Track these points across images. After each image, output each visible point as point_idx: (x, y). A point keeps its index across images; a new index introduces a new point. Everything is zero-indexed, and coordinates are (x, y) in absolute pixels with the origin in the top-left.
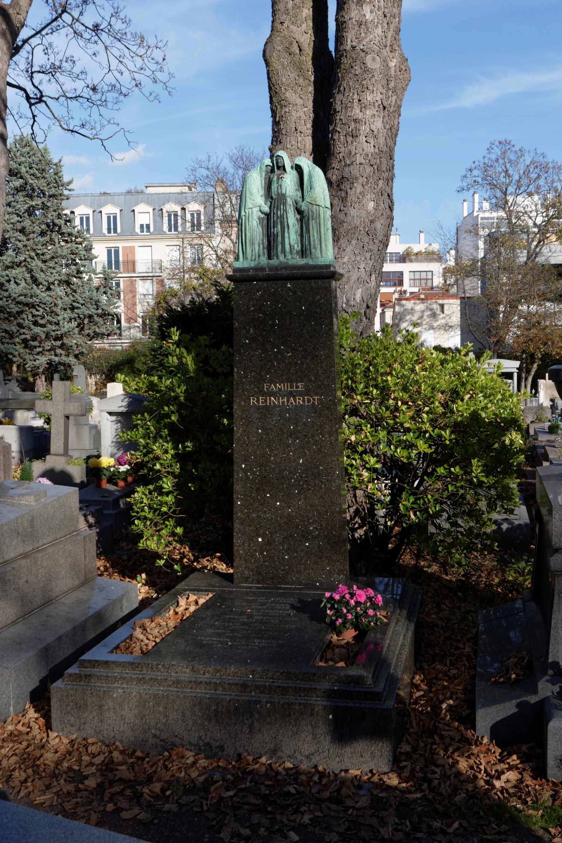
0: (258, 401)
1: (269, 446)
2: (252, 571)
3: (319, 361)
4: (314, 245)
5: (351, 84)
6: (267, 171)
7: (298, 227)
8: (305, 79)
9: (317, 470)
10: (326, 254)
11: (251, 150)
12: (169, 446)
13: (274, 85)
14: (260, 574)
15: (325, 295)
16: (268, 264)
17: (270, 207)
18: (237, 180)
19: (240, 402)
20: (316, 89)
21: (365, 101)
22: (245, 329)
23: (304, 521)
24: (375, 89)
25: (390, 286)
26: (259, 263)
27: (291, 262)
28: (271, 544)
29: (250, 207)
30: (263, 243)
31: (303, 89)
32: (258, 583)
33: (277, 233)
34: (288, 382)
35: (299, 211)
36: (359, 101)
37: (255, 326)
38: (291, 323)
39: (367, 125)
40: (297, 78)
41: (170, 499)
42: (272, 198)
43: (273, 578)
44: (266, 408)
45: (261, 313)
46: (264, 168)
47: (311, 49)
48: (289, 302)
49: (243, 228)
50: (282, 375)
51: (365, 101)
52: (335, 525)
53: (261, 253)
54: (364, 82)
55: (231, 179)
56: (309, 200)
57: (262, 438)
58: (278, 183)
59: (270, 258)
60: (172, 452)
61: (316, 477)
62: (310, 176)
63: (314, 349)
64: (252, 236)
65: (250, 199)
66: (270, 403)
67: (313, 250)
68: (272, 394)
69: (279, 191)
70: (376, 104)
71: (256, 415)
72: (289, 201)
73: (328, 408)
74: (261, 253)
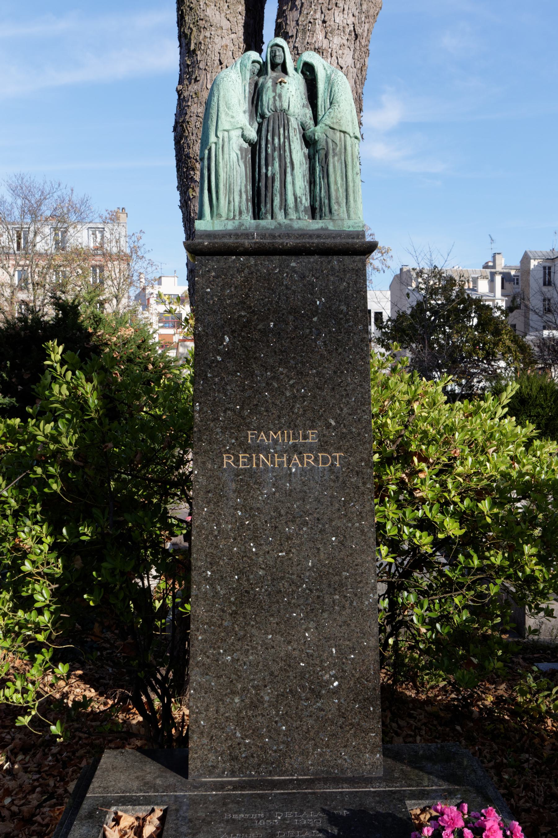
0: (237, 461)
1: (255, 539)
2: (221, 755)
3: (344, 393)
4: (337, 198)
7: (306, 167)
9: (337, 578)
10: (356, 214)
11: (32, 179)
12: (43, 530)
14: (234, 759)
15: (356, 283)
16: (257, 226)
17: (259, 132)
18: (15, 209)
19: (204, 463)
20: (247, 9)
21: (332, 23)
22: (216, 337)
23: (314, 665)
24: (346, 8)
25: (169, 327)
26: (241, 225)
27: (297, 225)
28: (256, 707)
30: (246, 192)
31: (231, 7)
32: (233, 773)
34: (289, 427)
35: (309, 142)
36: (324, 22)
37: (233, 332)
38: (296, 327)
39: (334, 58)
41: (45, 619)
42: (263, 116)
43: (259, 765)
44: (250, 473)
45: (243, 309)
48: (294, 292)
50: (279, 417)
51: (332, 23)
52: (368, 670)
53: (244, 208)
55: (9, 208)
56: (328, 122)
57: (242, 524)
58: (274, 91)
59: (257, 215)
60: (49, 540)
61: (335, 589)
62: (330, 82)
63: (335, 372)
64: (229, 178)
65: (227, 114)
66: (257, 465)
67: (335, 207)
68: (259, 448)
69: (278, 104)
70: (347, 31)
71: (233, 486)
72: (294, 124)
73: (357, 473)
74: (244, 208)
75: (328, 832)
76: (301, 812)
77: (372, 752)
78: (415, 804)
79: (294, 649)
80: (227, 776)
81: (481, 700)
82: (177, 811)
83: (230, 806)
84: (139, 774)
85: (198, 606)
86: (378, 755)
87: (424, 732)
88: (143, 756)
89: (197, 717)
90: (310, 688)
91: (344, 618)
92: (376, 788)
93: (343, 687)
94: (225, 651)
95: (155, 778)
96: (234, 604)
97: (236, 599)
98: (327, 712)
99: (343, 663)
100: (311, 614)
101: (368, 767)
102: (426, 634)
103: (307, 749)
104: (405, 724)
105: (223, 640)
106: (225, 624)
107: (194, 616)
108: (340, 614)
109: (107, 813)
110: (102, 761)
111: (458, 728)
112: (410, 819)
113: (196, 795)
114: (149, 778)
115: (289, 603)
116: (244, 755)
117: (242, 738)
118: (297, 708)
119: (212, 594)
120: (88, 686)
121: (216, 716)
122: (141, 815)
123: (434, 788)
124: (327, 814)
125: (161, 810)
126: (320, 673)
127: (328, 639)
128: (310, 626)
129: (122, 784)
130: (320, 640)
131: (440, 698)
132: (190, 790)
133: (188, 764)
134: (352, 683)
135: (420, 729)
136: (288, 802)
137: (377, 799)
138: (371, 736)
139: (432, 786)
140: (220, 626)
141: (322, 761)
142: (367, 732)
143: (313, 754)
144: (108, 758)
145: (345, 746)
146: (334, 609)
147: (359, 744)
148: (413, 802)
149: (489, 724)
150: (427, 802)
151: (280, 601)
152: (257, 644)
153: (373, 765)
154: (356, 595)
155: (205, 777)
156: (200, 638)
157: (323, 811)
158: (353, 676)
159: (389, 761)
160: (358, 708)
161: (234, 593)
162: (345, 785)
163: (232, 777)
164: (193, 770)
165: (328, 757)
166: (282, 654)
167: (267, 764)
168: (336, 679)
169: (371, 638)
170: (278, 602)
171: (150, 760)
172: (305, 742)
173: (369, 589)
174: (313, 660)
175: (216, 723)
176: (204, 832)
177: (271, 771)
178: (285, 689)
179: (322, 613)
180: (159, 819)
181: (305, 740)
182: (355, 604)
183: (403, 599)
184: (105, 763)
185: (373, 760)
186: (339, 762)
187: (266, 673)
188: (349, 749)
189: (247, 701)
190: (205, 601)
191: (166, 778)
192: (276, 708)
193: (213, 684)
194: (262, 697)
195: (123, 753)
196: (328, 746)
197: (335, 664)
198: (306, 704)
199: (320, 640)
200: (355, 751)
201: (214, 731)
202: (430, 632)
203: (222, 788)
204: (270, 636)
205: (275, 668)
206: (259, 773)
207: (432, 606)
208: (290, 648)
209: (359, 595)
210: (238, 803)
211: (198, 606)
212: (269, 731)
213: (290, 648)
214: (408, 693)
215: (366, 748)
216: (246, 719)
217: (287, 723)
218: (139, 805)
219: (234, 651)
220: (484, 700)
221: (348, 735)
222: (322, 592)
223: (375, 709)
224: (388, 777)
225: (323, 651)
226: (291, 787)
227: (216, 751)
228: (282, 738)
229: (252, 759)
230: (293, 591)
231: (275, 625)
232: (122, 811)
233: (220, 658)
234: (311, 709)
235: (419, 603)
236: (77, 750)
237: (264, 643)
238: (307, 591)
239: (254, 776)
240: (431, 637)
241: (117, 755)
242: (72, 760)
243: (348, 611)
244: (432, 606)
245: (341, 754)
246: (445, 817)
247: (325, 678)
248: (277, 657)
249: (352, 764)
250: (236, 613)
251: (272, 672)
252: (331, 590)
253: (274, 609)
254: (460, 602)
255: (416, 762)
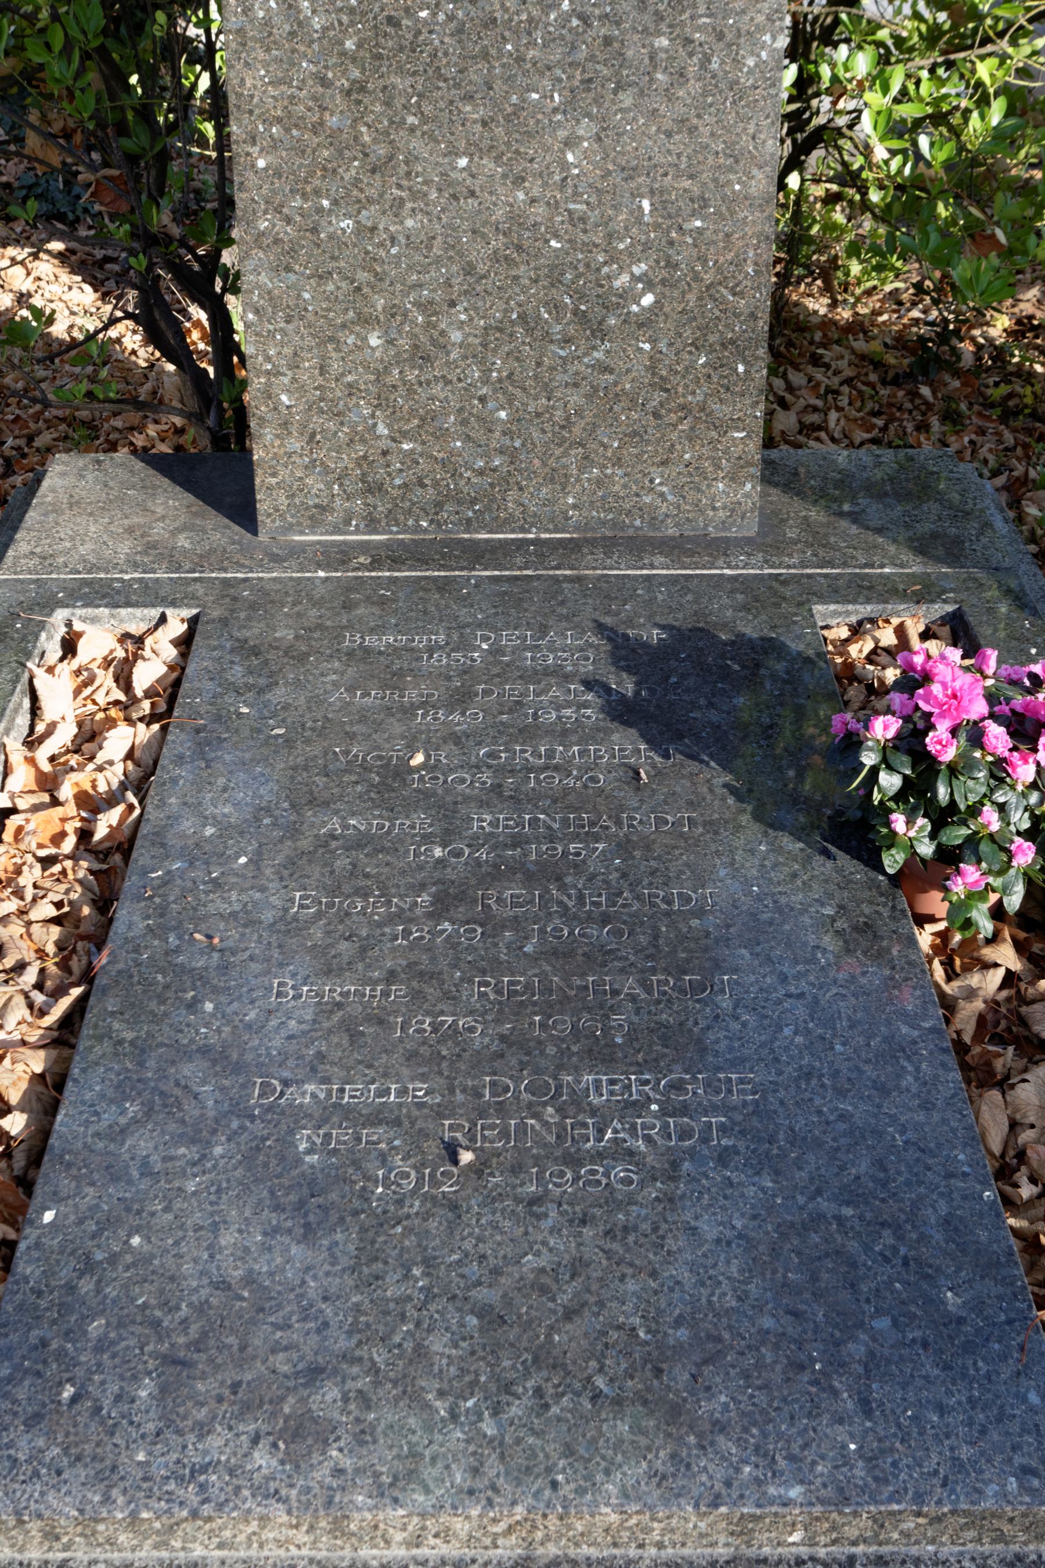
23: (589, 247)
32: (372, 524)
43: (439, 505)
52: (739, 263)
61: (659, 17)
75: (608, 690)
76: (543, 630)
77: (733, 478)
78: (835, 614)
79: (533, 201)
80: (357, 532)
81: (982, 325)
82: (224, 622)
83: (360, 611)
84: (136, 520)
85: (247, 64)
86: (748, 487)
87: (846, 401)
88: (152, 472)
89: (269, 384)
90: (576, 312)
91: (680, 109)
92: (737, 567)
93: (667, 309)
94: (335, 202)
95: (174, 533)
96: (354, 60)
97: (359, 45)
98: (619, 375)
99: (671, 243)
100: (585, 91)
101: (721, 513)
102: (886, 162)
103: (565, 467)
104: (804, 381)
105: (330, 172)
106: (333, 121)
107: (239, 95)
108: (669, 96)
109: (42, 626)
110: (46, 483)
111: (925, 391)
112: (822, 655)
113: (274, 579)
114: (159, 531)
115: (520, 59)
116: (398, 482)
117: (394, 440)
118: (539, 364)
119: (287, 28)
120: (79, 278)
121: (320, 380)
122: (136, 628)
123: (887, 570)
124: (610, 639)
125: (183, 621)
126: (605, 270)
127: (630, 172)
128: (581, 132)
129: (89, 546)
130: (609, 173)
131: (885, 317)
132: (261, 565)
133: (255, 501)
134: (692, 297)
135: (837, 392)
136: (510, 599)
137: (740, 597)
138: (734, 439)
139: (882, 566)
140: (317, 128)
141: (603, 498)
142: (723, 427)
143: (578, 480)
144: (64, 477)
145: (664, 463)
146: (652, 80)
147: (700, 457)
148: (832, 607)
149: (996, 384)
150: (869, 608)
151: (493, 52)
152: (426, 182)
153: (733, 509)
154: (720, 36)
155: (302, 533)
156: (261, 163)
157: (600, 628)
158: (697, 278)
159: (775, 494)
160: (703, 366)
161: (352, 24)
162: (659, 559)
163: (370, 533)
164: (269, 515)
165: (617, 488)
166: (499, 214)
167: (460, 502)
168: (650, 286)
169: (755, 172)
170: (485, 55)
171: (166, 481)
172: (558, 452)
173: (760, 18)
174: (585, 231)
175: (322, 399)
176: (286, 685)
177: (469, 521)
178: (506, 311)
179: (615, 92)
180: (177, 643)
181: (560, 445)
182: (715, 65)
183: (833, 65)
184: (53, 490)
185: (734, 496)
186: (647, 500)
187: (455, 268)
188: (673, 470)
189: (404, 343)
190: (268, 50)
191: (205, 532)
192: (483, 362)
193: (306, 296)
194: (443, 333)
195: (99, 462)
196: (618, 462)
197: (647, 246)
198: (562, 353)
199: (609, 173)
200: (690, 475)
201: (317, 421)
202: (899, 159)
203: (343, 562)
204: (463, 162)
205: (479, 254)
206: (439, 525)
207: (911, 88)
208: (521, 196)
209: (729, 37)
210: (383, 602)
211: (247, 64)
212: (464, 422)
213: (521, 196)
214: (811, 304)
215: (719, 467)
216: (402, 391)
217: (510, 402)
218: (128, 604)
219: (361, 205)
220: (988, 324)
221: (674, 436)
222: (618, 24)
223: (752, 369)
224: (769, 540)
225: (614, 207)
226: (519, 560)
227: (326, 470)
228: (497, 439)
229: (419, 491)
230: (530, 20)
231: (478, 127)
232: (83, 620)
233: (324, 223)
234: (576, 366)
235: (879, 79)
236: (39, 433)
237: (447, 183)
238: (575, 22)
239: (425, 531)
240: (900, 171)
241: (85, 468)
242: (24, 456)
243: (694, 87)
244: (911, 88)
245: (652, 481)
246: (936, 689)
247: (617, 284)
248: (485, 223)
249: (678, 507)
250: (363, 89)
251: (470, 264)
252: (647, 19)
253: (474, 77)
254: (992, 75)
255: (835, 492)
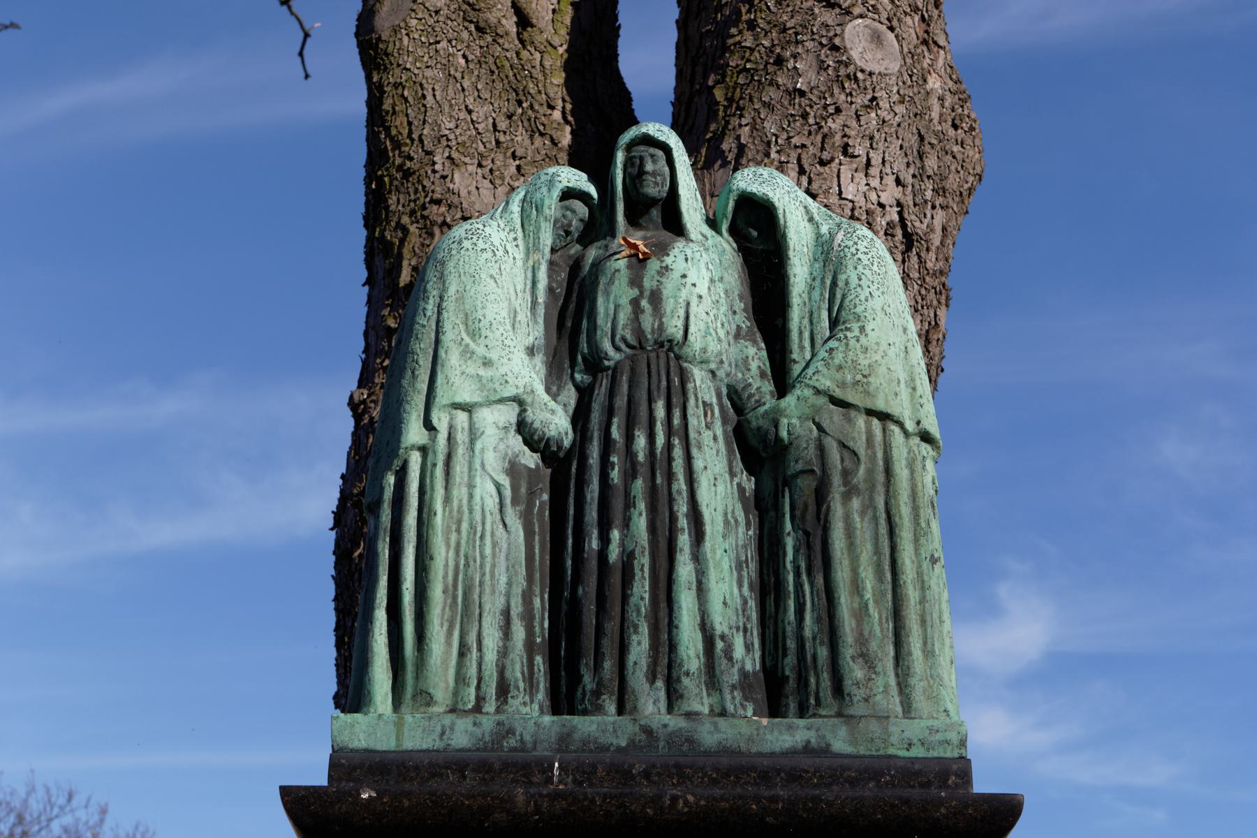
4: (862, 640)
5: (771, 127)
6: (563, 231)
7: (744, 534)
8: (535, 131)
10: (934, 698)
13: (397, 145)
16: (564, 739)
24: (876, 159)
27: (710, 735)
29: (465, 396)
30: (528, 617)
33: (628, 558)
35: (757, 449)
40: (503, 125)
42: (594, 364)
46: (551, 203)
47: (563, 32)
49: (411, 519)
53: (516, 672)
54: (834, 125)
56: (825, 383)
58: (636, 282)
59: (564, 698)
67: (855, 672)
69: (647, 322)
72: (702, 385)
74: (516, 672)
